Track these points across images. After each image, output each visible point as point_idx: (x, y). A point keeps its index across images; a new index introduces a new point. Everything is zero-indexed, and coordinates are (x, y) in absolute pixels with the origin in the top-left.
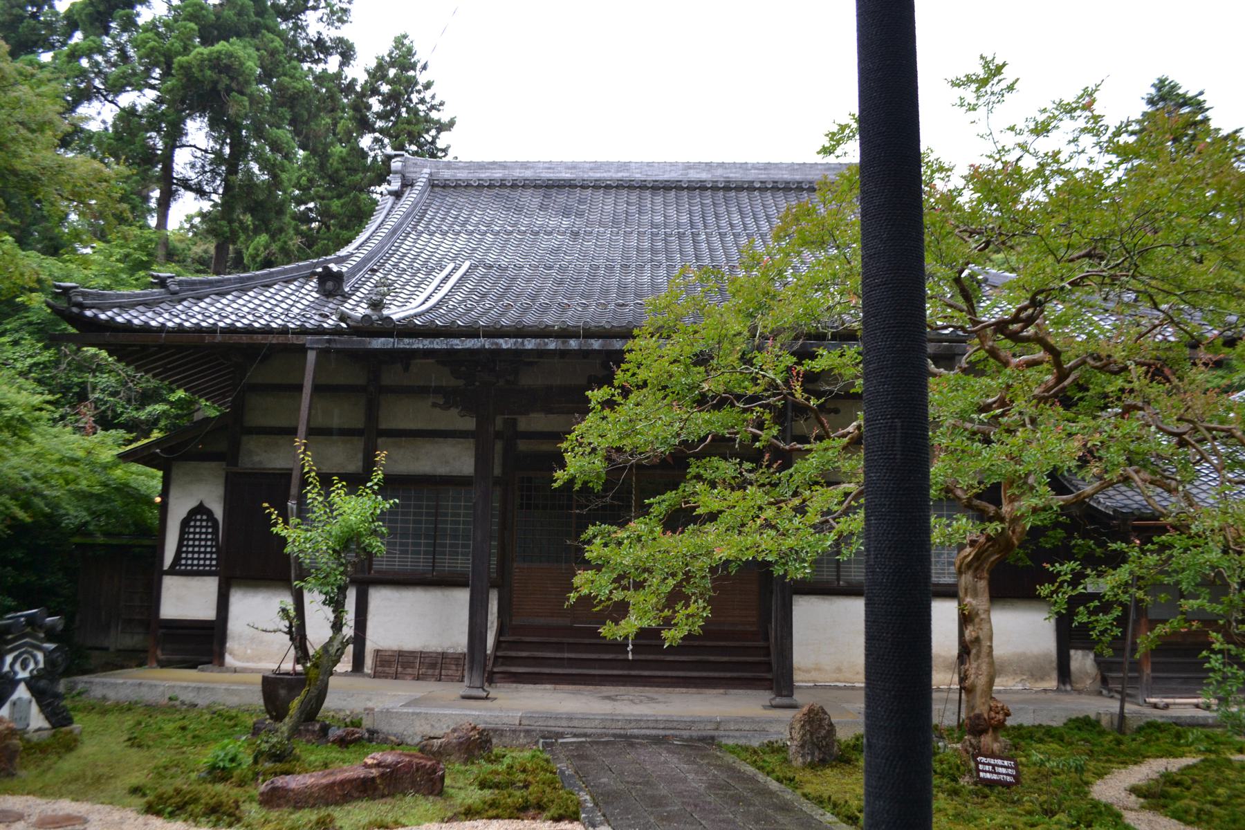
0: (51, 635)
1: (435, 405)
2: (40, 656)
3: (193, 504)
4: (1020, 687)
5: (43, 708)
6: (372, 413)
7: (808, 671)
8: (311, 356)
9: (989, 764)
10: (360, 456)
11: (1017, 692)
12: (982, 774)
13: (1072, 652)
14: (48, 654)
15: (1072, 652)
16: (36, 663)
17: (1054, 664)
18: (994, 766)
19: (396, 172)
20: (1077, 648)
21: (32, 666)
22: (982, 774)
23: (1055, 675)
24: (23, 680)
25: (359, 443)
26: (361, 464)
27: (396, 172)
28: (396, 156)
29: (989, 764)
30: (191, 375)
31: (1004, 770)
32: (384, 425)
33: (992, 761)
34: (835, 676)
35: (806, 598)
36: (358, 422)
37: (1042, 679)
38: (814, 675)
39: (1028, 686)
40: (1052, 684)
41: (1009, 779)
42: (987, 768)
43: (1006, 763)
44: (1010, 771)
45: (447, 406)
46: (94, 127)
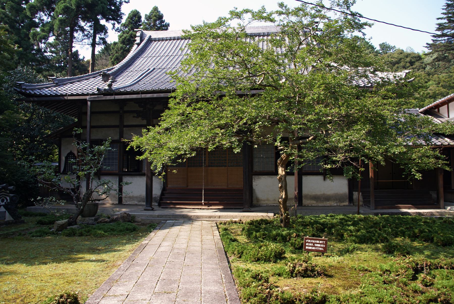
0: (11, 192)
1: (134, 117)
2: (8, 198)
3: (69, 151)
4: (336, 205)
5: (10, 214)
6: (121, 119)
7: (264, 201)
8: (89, 103)
9: (312, 243)
10: (118, 134)
11: (335, 206)
12: (307, 247)
13: (354, 193)
14: (11, 198)
15: (354, 193)
16: (7, 200)
17: (348, 197)
18: (314, 244)
19: (138, 37)
20: (356, 191)
21: (5, 201)
22: (307, 247)
23: (347, 200)
24: (3, 205)
25: (118, 130)
26: (118, 137)
27: (138, 37)
28: (138, 31)
29: (312, 243)
30: (68, 109)
31: (319, 245)
32: (125, 124)
33: (314, 241)
34: (273, 202)
35: (264, 176)
36: (117, 123)
37: (343, 202)
38: (266, 202)
39: (338, 204)
40: (347, 203)
41: (321, 249)
42: (310, 244)
43: (321, 242)
44: (322, 245)
45: (137, 117)
46: (76, 47)
